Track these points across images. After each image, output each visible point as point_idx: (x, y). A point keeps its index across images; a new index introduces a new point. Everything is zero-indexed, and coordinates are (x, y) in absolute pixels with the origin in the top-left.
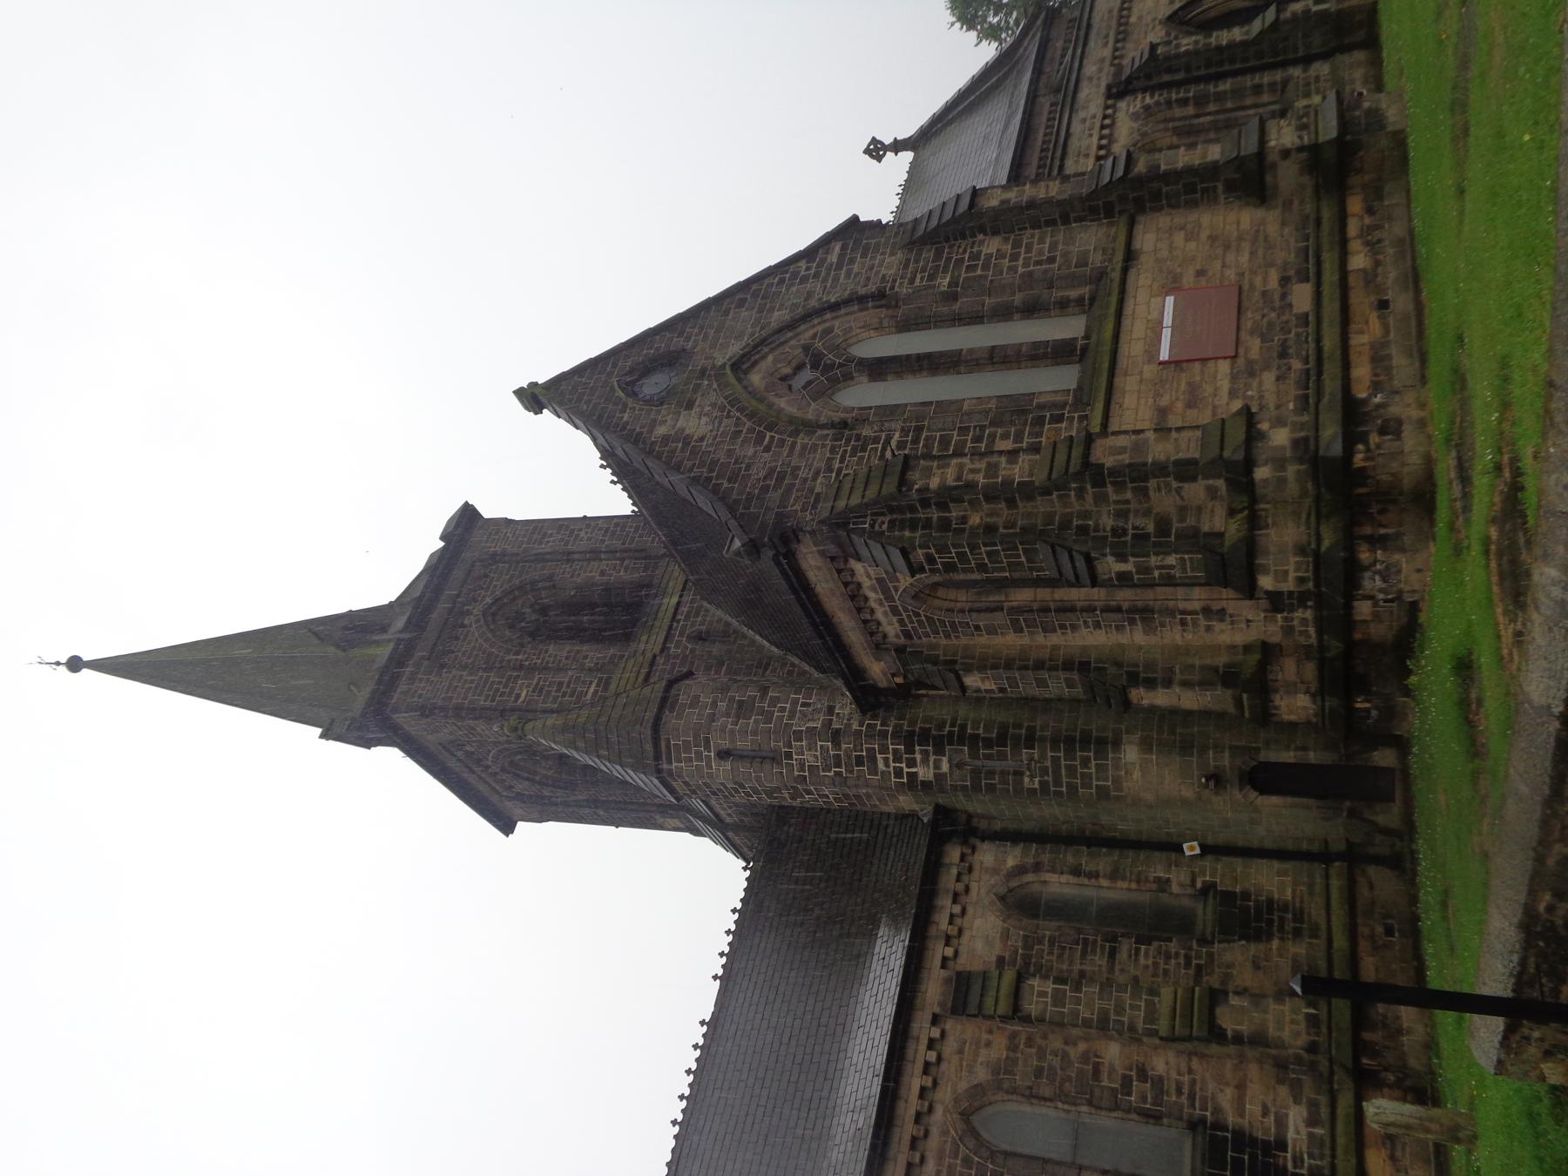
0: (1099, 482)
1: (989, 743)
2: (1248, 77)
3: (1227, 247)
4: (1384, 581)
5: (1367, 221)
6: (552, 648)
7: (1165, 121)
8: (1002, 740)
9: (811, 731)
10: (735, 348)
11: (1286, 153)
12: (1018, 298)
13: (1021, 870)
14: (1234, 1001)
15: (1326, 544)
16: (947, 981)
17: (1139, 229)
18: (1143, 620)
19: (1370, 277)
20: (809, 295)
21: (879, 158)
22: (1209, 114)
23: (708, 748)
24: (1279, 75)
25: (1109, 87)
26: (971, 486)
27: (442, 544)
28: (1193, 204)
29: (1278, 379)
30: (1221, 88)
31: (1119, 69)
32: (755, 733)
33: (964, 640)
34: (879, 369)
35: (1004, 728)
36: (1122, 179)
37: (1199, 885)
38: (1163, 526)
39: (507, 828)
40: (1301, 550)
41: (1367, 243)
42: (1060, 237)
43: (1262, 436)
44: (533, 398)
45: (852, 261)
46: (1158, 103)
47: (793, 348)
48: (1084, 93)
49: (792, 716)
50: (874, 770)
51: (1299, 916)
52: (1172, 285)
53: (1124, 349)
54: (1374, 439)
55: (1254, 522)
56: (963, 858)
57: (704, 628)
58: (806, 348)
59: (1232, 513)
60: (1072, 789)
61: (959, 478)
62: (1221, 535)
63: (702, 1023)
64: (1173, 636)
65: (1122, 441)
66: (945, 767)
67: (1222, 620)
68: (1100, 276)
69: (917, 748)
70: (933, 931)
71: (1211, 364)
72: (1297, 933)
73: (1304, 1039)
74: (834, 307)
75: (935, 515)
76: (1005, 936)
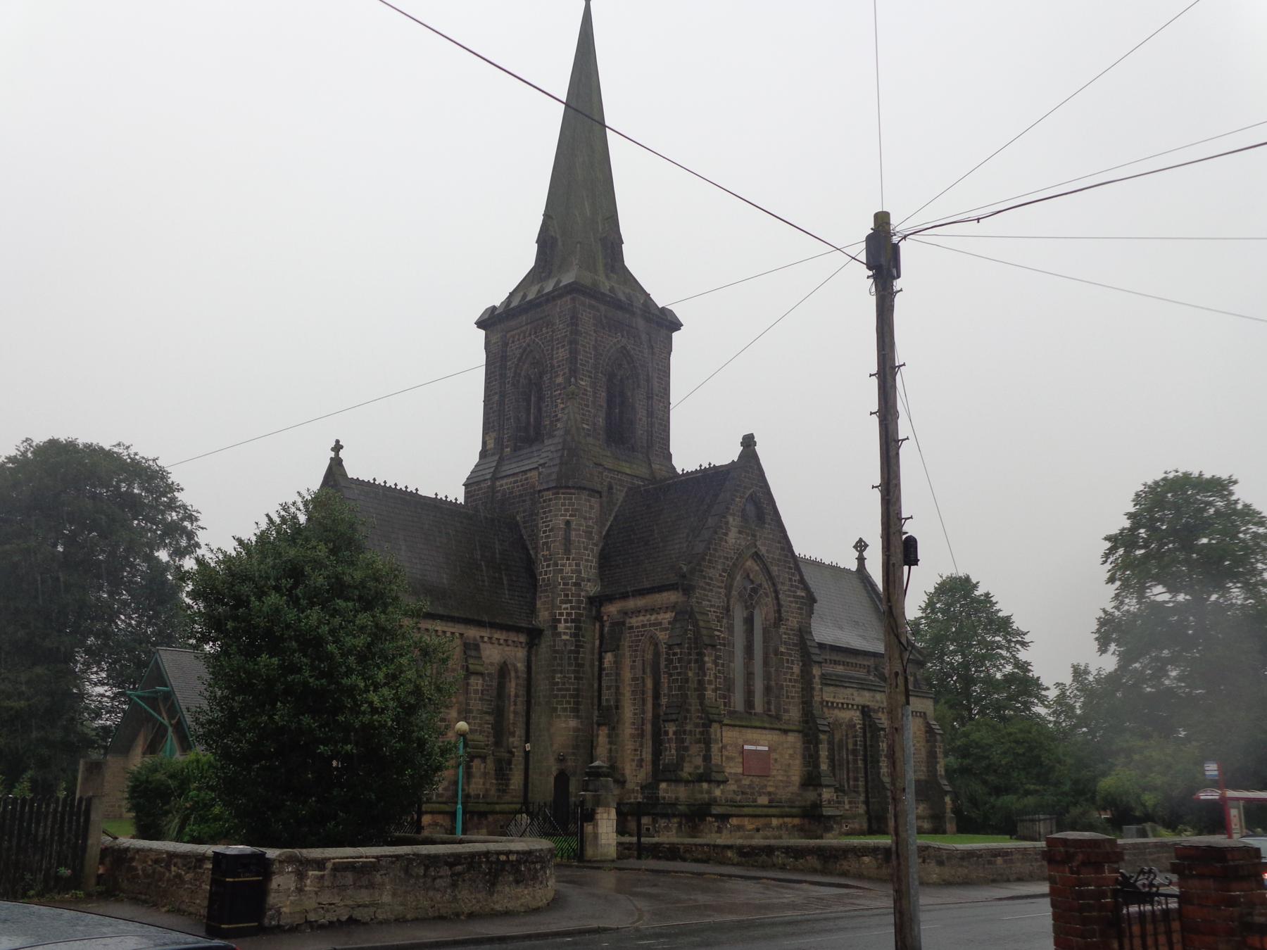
0: (704, 725)
1: (576, 659)
2: (863, 775)
3: (786, 771)
4: (664, 827)
5: (790, 825)
6: (604, 394)
7: (847, 735)
8: (578, 665)
9: (580, 572)
10: (763, 550)
11: (820, 795)
12: (773, 683)
13: (516, 671)
14: (483, 766)
15: (679, 807)
16: (475, 639)
17: (796, 734)
18: (638, 734)
19: (768, 826)
20: (783, 584)
21: (855, 547)
22: (847, 756)
23: (571, 516)
24: (861, 789)
25: (868, 706)
26: (705, 675)
27: (660, 306)
28: (804, 757)
29: (734, 791)
30: (859, 762)
31: (876, 711)
32: (579, 542)
33: (627, 654)
34: (749, 621)
35: (582, 665)
36: (818, 728)
37: (513, 750)
38: (686, 749)
39: (481, 324)
40: (677, 799)
41: (781, 825)
42: (796, 700)
43: (719, 786)
44: (748, 442)
45: (796, 603)
46: (856, 731)
47: (761, 579)
48: (867, 694)
49: (587, 561)
50: (562, 602)
51: (504, 791)
52: (772, 749)
53: (749, 730)
54: (716, 824)
55: (687, 782)
56: (521, 643)
57: (614, 491)
58: (760, 585)
59: (690, 774)
60: (556, 696)
61: (708, 669)
62: (682, 770)
63: (417, 490)
64: (629, 746)
65: (719, 734)
66: (564, 637)
67: (637, 766)
68: (778, 718)
69: (573, 625)
70: (494, 631)
71: (741, 765)
72: (499, 790)
73: (472, 793)
74: (777, 598)
75: (693, 657)
76: (492, 664)
